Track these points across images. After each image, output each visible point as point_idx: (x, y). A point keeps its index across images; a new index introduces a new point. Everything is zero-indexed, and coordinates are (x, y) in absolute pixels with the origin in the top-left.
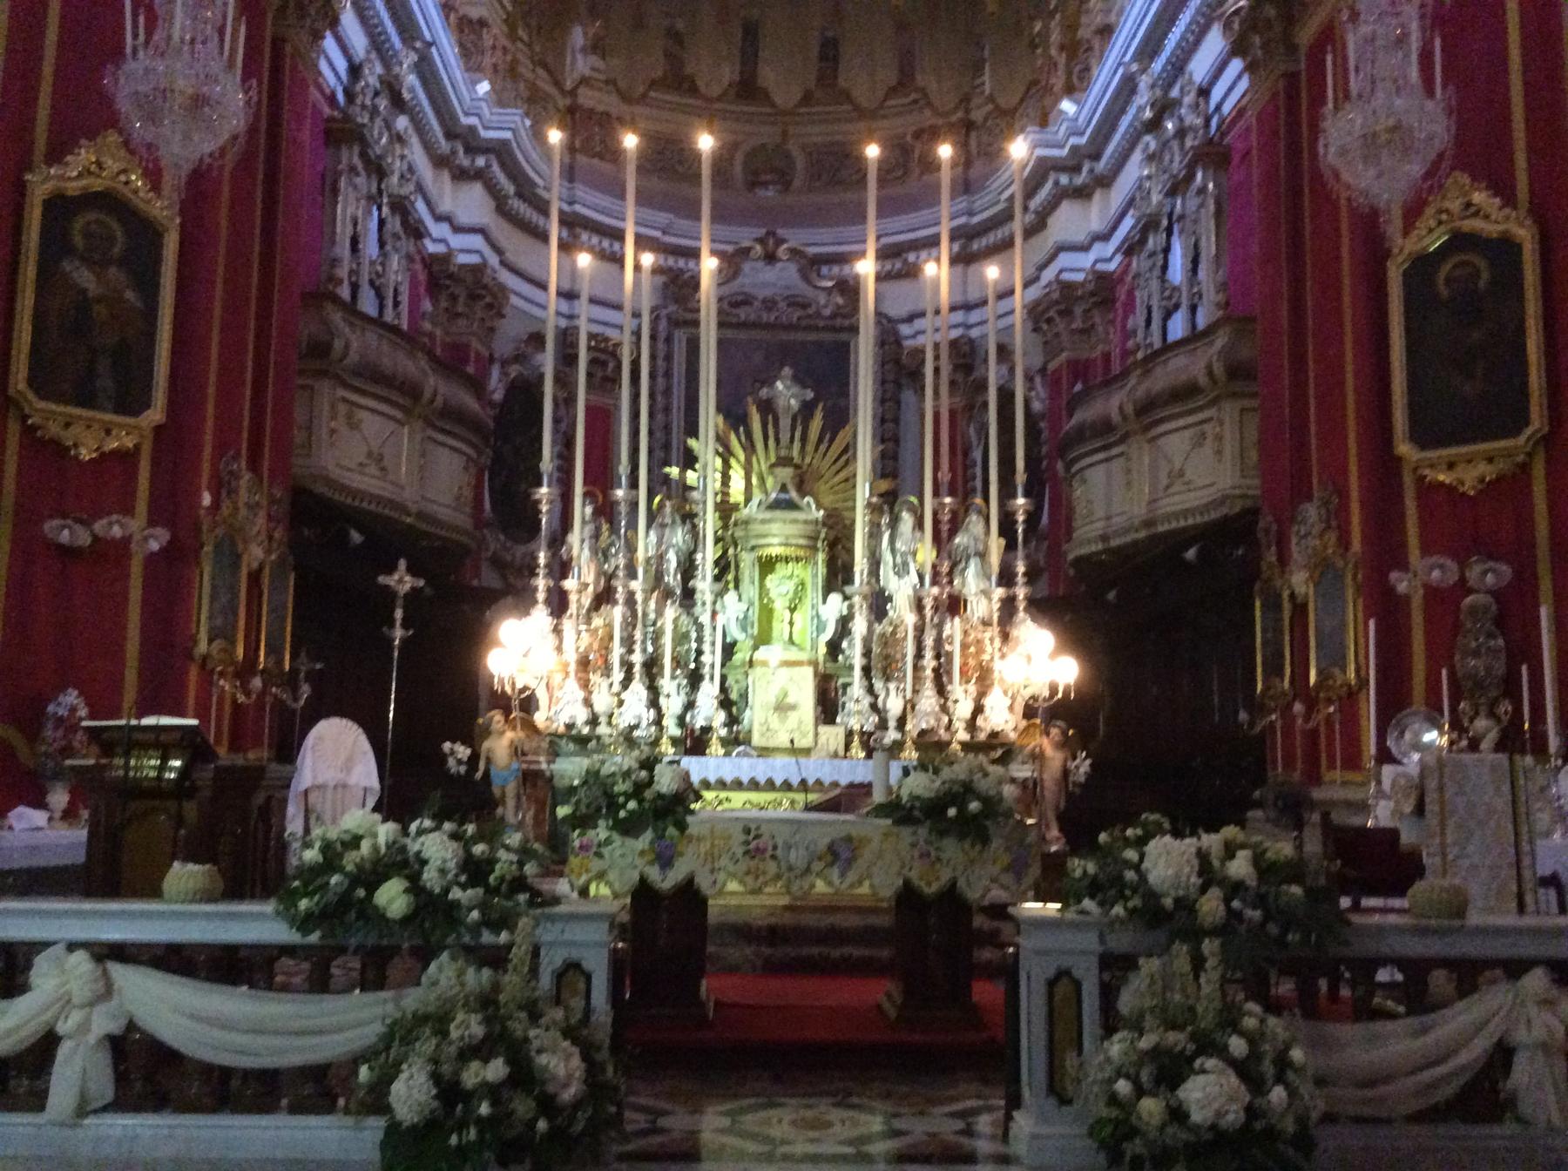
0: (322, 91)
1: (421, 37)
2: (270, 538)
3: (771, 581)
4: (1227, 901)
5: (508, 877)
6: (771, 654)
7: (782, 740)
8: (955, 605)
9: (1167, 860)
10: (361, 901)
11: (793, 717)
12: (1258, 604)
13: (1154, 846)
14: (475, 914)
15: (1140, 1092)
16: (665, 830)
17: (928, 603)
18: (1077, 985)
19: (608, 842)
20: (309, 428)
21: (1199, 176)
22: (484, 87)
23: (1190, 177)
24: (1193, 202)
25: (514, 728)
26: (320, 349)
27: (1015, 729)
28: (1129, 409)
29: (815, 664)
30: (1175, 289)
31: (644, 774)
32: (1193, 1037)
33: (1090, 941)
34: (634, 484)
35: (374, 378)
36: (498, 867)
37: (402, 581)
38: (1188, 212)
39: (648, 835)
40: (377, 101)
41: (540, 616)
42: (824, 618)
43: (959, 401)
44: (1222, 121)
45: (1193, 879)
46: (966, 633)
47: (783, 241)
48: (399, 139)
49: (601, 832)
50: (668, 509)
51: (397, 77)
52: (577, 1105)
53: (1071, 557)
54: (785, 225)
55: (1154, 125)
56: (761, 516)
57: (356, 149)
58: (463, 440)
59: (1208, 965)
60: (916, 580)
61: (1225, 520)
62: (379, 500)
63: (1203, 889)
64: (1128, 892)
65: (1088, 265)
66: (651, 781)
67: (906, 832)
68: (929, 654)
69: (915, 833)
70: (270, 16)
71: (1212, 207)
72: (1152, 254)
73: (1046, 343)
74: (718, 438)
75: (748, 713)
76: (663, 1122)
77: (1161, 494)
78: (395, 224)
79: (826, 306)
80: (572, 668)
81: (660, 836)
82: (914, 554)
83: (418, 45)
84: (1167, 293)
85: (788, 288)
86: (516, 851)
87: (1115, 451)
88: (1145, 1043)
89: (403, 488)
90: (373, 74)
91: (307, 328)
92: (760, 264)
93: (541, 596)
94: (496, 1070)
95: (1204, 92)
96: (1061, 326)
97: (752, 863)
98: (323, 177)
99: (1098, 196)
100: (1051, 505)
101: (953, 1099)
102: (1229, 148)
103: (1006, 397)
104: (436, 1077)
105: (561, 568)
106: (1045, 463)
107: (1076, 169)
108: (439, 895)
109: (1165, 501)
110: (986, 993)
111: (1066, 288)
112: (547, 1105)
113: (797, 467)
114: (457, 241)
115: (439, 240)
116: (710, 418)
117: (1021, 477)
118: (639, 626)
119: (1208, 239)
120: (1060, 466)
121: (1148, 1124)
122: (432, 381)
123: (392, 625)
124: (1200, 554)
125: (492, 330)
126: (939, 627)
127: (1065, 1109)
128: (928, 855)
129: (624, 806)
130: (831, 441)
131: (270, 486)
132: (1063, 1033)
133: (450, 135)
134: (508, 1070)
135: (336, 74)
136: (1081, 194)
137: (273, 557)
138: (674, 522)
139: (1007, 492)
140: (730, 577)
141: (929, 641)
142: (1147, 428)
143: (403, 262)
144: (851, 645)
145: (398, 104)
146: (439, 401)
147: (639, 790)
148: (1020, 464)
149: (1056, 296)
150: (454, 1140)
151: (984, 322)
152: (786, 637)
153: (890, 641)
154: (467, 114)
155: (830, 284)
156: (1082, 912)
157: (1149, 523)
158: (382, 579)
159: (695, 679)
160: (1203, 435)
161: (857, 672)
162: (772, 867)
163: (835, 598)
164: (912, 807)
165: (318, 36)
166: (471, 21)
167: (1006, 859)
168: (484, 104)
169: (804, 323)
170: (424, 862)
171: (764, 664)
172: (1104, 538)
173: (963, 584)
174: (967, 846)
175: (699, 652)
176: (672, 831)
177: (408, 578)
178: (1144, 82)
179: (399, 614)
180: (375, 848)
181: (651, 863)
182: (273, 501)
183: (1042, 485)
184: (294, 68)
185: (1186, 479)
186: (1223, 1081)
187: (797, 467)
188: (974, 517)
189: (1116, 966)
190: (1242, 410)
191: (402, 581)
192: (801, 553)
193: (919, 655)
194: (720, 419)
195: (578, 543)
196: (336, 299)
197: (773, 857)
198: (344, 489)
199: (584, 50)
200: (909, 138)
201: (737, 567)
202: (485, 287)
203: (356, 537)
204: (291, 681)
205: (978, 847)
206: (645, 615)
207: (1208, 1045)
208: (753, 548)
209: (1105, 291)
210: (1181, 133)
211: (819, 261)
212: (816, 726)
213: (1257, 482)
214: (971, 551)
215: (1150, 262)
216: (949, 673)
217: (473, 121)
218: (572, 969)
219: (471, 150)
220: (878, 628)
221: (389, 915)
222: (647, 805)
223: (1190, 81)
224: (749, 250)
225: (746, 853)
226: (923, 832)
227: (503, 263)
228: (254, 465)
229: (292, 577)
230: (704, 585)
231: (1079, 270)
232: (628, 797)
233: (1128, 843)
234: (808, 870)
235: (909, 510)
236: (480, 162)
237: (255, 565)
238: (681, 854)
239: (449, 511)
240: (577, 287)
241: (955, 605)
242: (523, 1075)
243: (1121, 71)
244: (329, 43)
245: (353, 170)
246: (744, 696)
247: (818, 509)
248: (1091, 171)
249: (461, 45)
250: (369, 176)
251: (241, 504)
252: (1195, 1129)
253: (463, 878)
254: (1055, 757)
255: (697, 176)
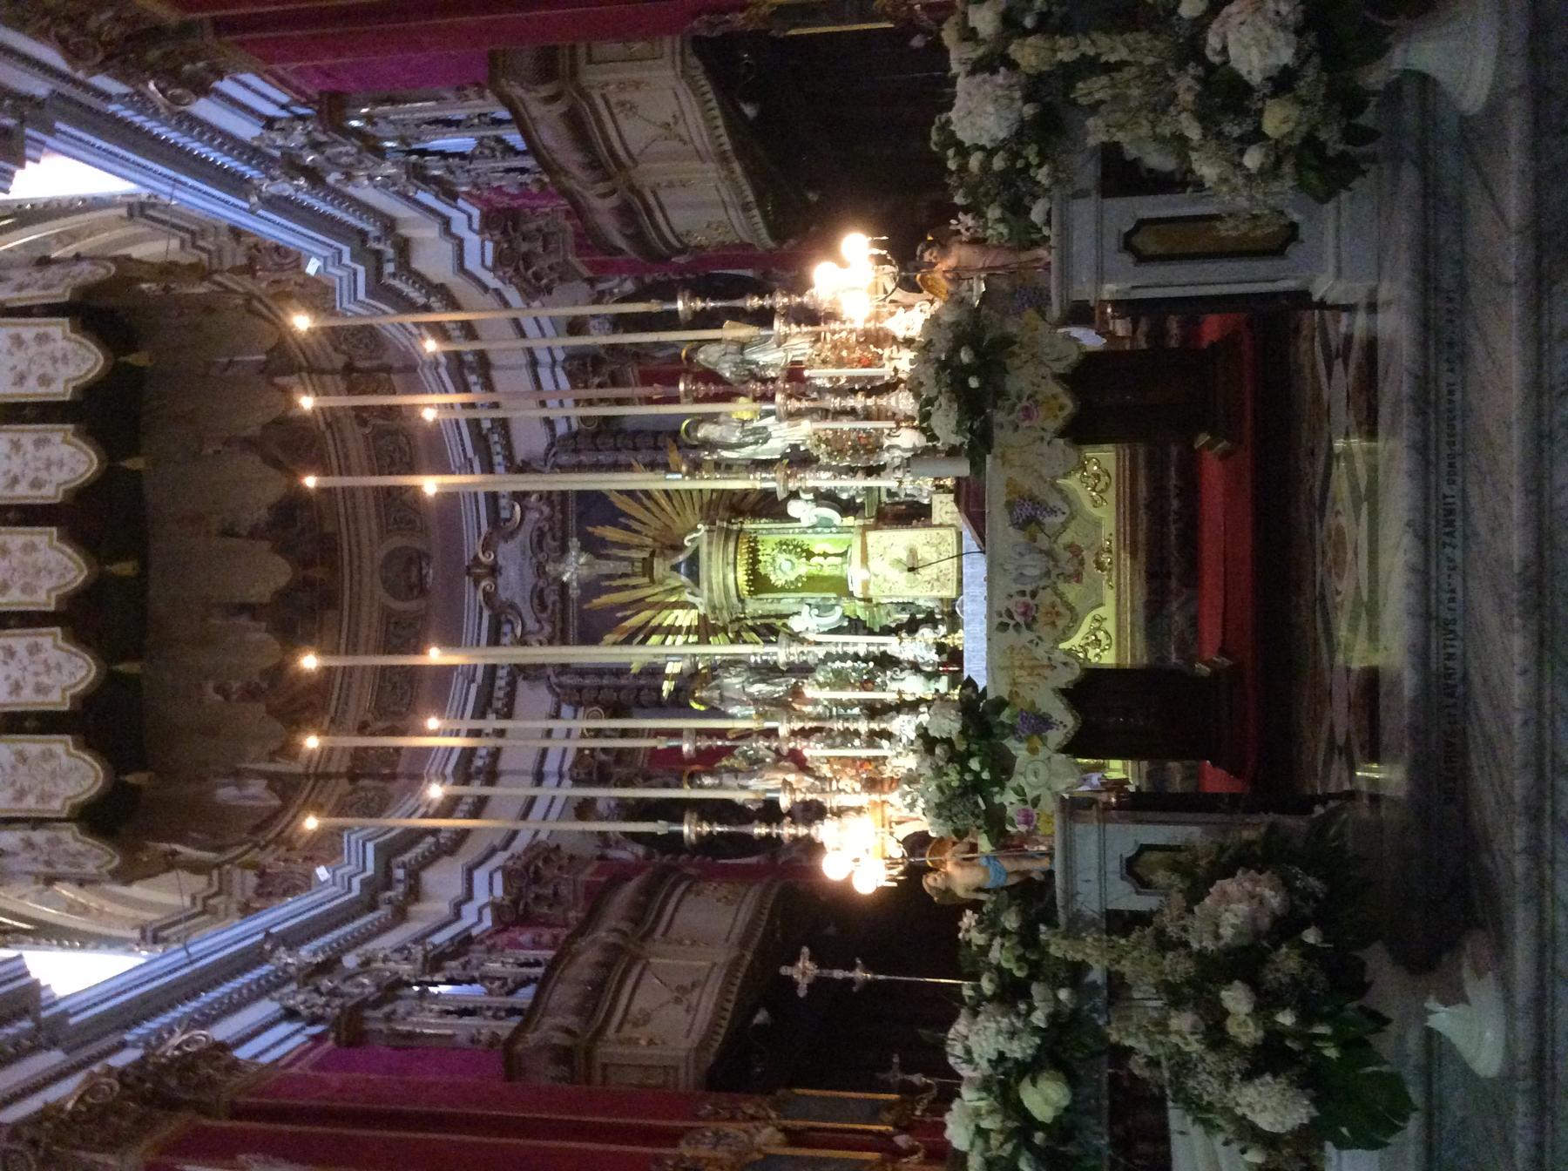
0: (311, 1049)
1: (260, 944)
2: (753, 1118)
3: (777, 579)
4: (1027, 33)
5: (1020, 951)
6: (857, 578)
7: (950, 566)
8: (794, 373)
9: (979, 115)
10: (1049, 1136)
11: (926, 553)
12: (793, 32)
13: (965, 135)
14: (1063, 994)
15: (1257, 136)
16: (1002, 724)
17: (794, 405)
18: (1141, 224)
19: (1020, 791)
20: (647, 1068)
21: (355, 123)
22: (322, 873)
23: (356, 132)
24: (384, 129)
25: (944, 863)
26: (563, 1056)
27: (932, 302)
28: (602, 187)
29: (865, 528)
30: (481, 142)
31: (938, 751)
32: (1181, 66)
33: (1084, 211)
34: (676, 733)
35: (597, 997)
36: (1005, 965)
37: (803, 970)
38: (396, 134)
39: (1011, 743)
40: (323, 989)
41: (823, 831)
42: (814, 521)
43: (632, 372)
44: (297, 103)
45: (1000, 79)
46: (824, 362)
47: (476, 557)
48: (366, 963)
49: (1008, 799)
50: (704, 694)
51: (299, 969)
52: (1287, 884)
53: (771, 244)
54: (462, 559)
55: (314, 176)
56: (706, 592)
57: (369, 1013)
58: (668, 896)
59: (1091, 52)
60: (772, 419)
61: (710, 71)
62: (724, 992)
63: (1012, 65)
64: (1020, 164)
65: (476, 239)
66: (948, 741)
67: (999, 436)
68: (850, 402)
69: (1002, 426)
70: (207, 1122)
71: (387, 108)
72: (450, 170)
73: (561, 279)
74: (628, 641)
75: (920, 602)
76: (1341, 740)
77: (690, 147)
78: (453, 966)
79: (541, 512)
80: (875, 797)
81: (1013, 730)
82: (743, 422)
83: (268, 947)
84: (487, 152)
85: (523, 553)
86: (993, 936)
87: (651, 200)
88: (1194, 133)
89: (714, 964)
90: (297, 997)
91: (545, 1074)
92: (500, 581)
93: (802, 831)
94: (1236, 999)
95: (270, 123)
96: (542, 264)
97: (1041, 618)
98: (396, 1048)
99: (404, 231)
100: (730, 267)
101: (1316, 377)
102: (321, 93)
103: (622, 323)
104: (1248, 1076)
105: (770, 811)
106: (688, 276)
107: (378, 255)
108: (1042, 1038)
109: (698, 142)
110: (1212, 328)
111: (501, 261)
112: (1286, 927)
113: (653, 554)
114: (481, 896)
115: (476, 919)
116: (605, 653)
117: (654, 306)
118: (828, 725)
119: (420, 110)
120: (681, 260)
121: (1298, 124)
122: (602, 934)
123: (851, 982)
124: (749, 100)
125: (572, 858)
126: (821, 391)
127: (1304, 232)
128: (1026, 409)
129: (977, 774)
130: (625, 515)
131: (697, 1117)
132: (1191, 241)
133: (373, 907)
134: (1237, 983)
135: (293, 1034)
136: (404, 248)
137: (773, 1115)
138: (718, 687)
139: (670, 321)
140: (779, 623)
141: (834, 402)
142: (620, 165)
143: (493, 957)
144: (843, 490)
145: (328, 966)
146: (624, 926)
147: (959, 759)
148: (640, 307)
149: (510, 271)
150: (1332, 1052)
151: (550, 350)
152: (839, 560)
153: (836, 445)
154: (350, 890)
155: (518, 508)
156: (1048, 222)
157: (723, 159)
158: (802, 993)
159: (886, 662)
160: (622, 104)
161: (872, 482)
162: (1046, 597)
163: (794, 508)
164: (971, 430)
165: (235, 1065)
166: (260, 886)
167: (1030, 314)
168: (339, 873)
169: (559, 534)
170: (1002, 1056)
171: (866, 585)
172: (746, 208)
173: (775, 366)
174: (1017, 362)
175: (856, 657)
176: (1005, 716)
177: (800, 965)
178: (268, 188)
179: (839, 974)
180: (991, 1112)
181: (1044, 740)
182: (716, 1116)
183: (710, 277)
184: (263, 1093)
185: (671, 120)
186: (1236, 20)
187: (653, 554)
188: (701, 357)
189: (1121, 175)
190: (590, 61)
191: (803, 970)
192: (743, 548)
193: (852, 413)
194: (609, 638)
195: (747, 792)
196: (518, 1032)
197: (1034, 594)
198: (713, 1026)
199: (239, 787)
200: (367, 431)
201: (768, 617)
202: (526, 868)
203: (761, 1017)
204: (909, 1090)
205: (1016, 348)
206: (819, 718)
207: (1191, 49)
208: (741, 601)
209: (500, 219)
210: (316, 146)
211: (495, 519)
212: (931, 526)
213: (668, 40)
214: (738, 358)
215: (458, 172)
216: (871, 379)
217: (356, 883)
218: (1134, 870)
219: (388, 884)
220: (824, 460)
221: (1065, 1103)
222: (974, 747)
223: (260, 138)
224: (486, 593)
225: (1029, 627)
226: (999, 417)
227: (505, 847)
228: (672, 1137)
229: (799, 1091)
230: (782, 653)
231: (483, 247)
232: (965, 768)
233: (963, 168)
234: (1049, 554)
235: (696, 430)
236: (400, 873)
237: (780, 1136)
238: (1033, 704)
239: (744, 907)
240: (502, 780)
241: (794, 373)
242: (1243, 962)
243: (261, 212)
244: (243, 1053)
245: (388, 1018)
246: (903, 606)
247: (697, 530)
248: (378, 239)
249: (285, 893)
250: (401, 998)
251: (712, 1154)
252: (1302, 57)
253: (1022, 1007)
254: (957, 255)
255: (348, 671)
